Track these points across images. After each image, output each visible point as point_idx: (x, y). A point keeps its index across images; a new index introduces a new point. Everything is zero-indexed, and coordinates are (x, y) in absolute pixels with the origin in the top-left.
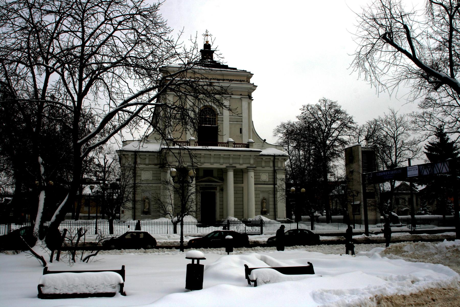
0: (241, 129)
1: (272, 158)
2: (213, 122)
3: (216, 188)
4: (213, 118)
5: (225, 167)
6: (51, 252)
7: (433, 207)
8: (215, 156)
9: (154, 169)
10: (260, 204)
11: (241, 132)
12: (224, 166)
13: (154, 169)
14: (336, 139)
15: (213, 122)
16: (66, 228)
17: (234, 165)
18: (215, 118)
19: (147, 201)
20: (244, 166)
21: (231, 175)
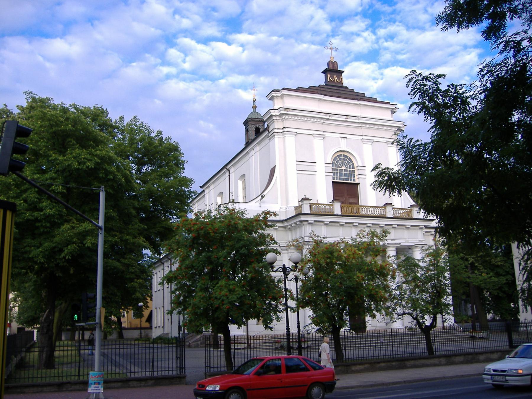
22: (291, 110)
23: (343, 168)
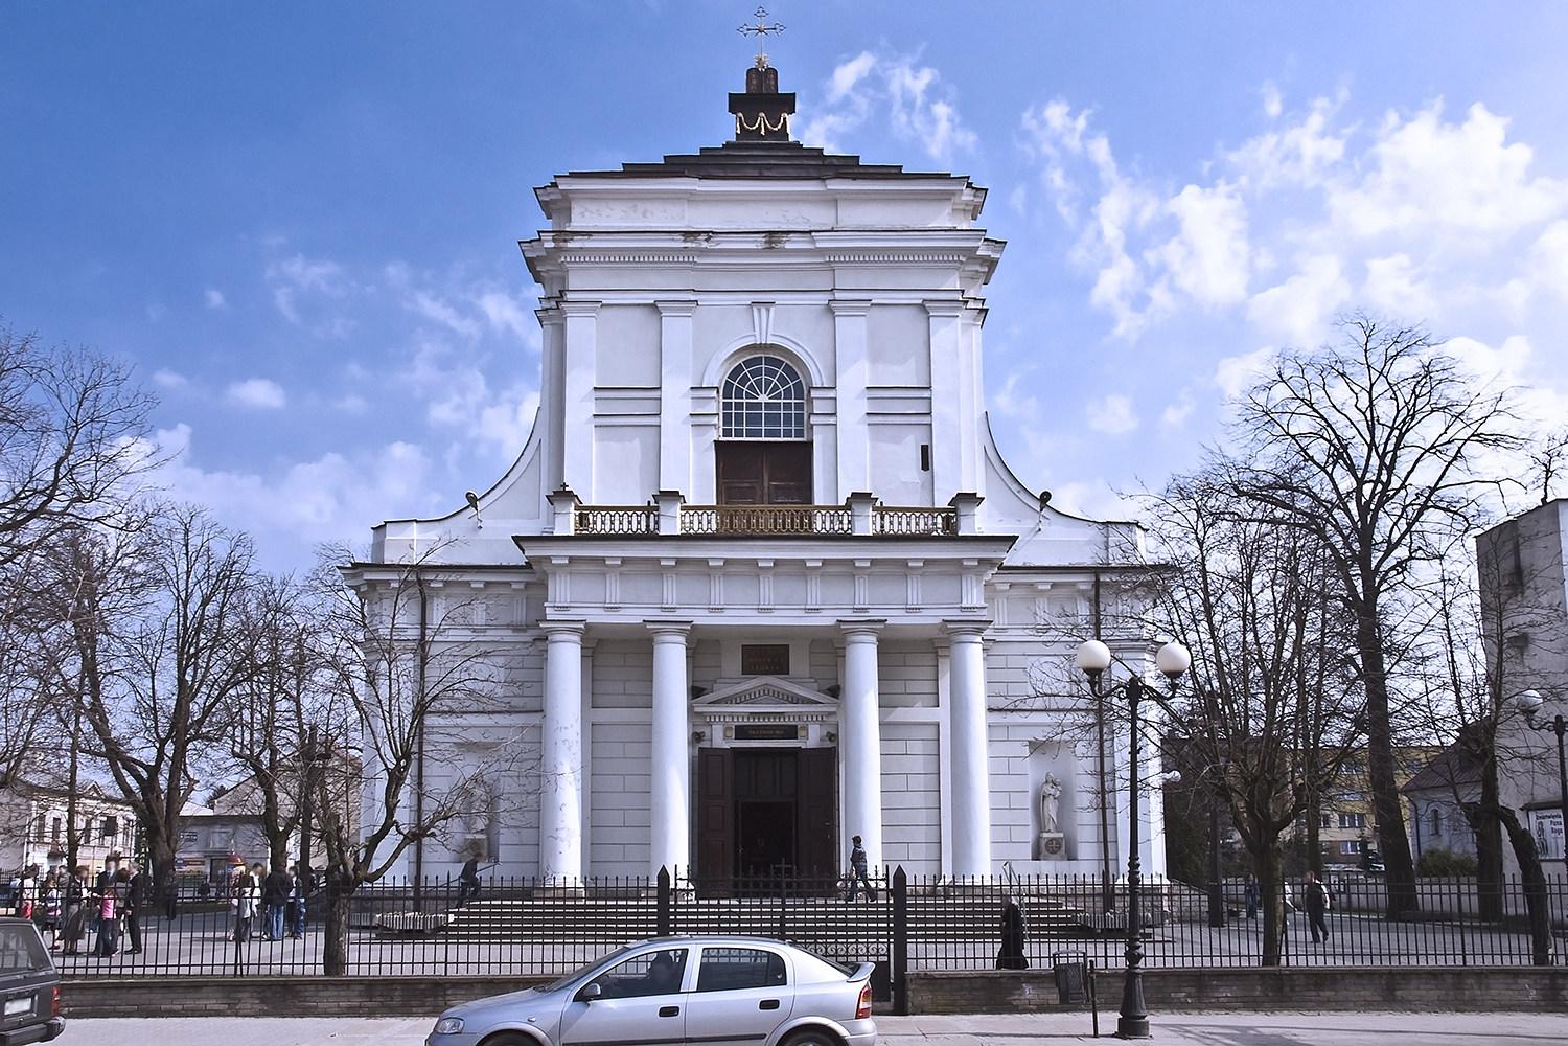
0: (925, 451)
1: (1084, 582)
2: (739, 417)
3: (805, 728)
4: (788, 406)
5: (831, 622)
6: (891, 1009)
7: (12, 1040)
8: (731, 569)
9: (969, 587)
10: (1029, 804)
11: (926, 464)
12: (826, 619)
13: (969, 587)
14: (1429, 499)
15: (739, 417)
16: (104, 961)
17: (874, 614)
18: (799, 406)
19: (479, 791)
20: (930, 618)
21: (864, 659)
22: (595, 237)
23: (763, 398)
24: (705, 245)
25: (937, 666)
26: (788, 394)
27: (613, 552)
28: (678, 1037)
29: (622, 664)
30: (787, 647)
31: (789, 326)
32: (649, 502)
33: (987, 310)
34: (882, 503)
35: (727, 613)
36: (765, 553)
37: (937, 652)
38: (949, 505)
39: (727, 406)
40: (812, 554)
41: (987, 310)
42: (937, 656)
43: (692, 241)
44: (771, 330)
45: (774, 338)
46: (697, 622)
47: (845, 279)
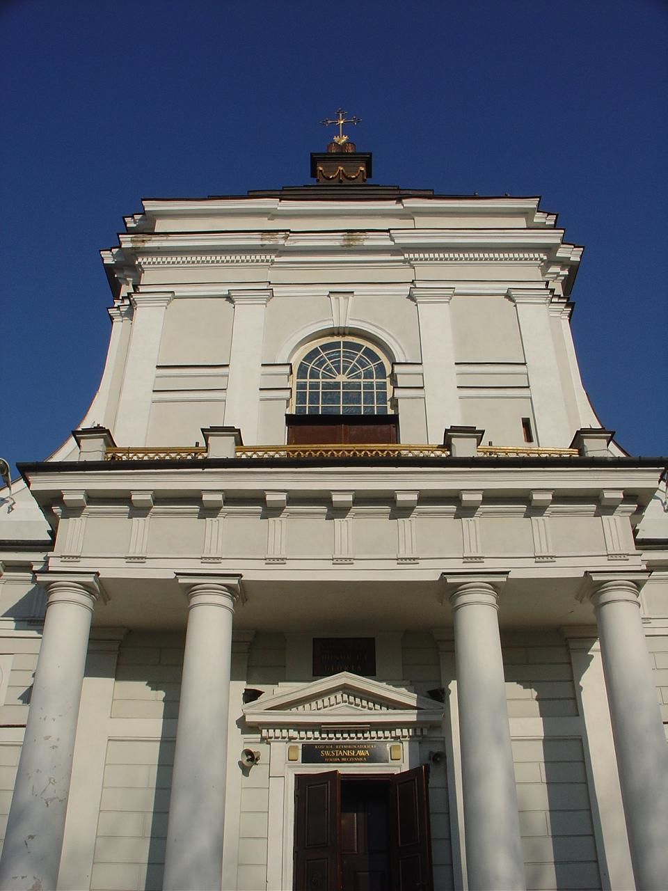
23: (341, 378)
24: (282, 242)
25: (570, 663)
26: (369, 375)
27: (141, 484)
28: (432, 834)
29: (243, 786)
30: (371, 641)
31: (371, 306)
32: (197, 444)
33: (574, 303)
34: (490, 444)
35: (290, 564)
36: (341, 483)
37: (567, 645)
38: (570, 448)
39: (301, 386)
40: (406, 484)
41: (574, 303)
42: (568, 652)
43: (269, 239)
44: (344, 314)
45: (350, 321)
46: (247, 576)
47: (423, 272)
